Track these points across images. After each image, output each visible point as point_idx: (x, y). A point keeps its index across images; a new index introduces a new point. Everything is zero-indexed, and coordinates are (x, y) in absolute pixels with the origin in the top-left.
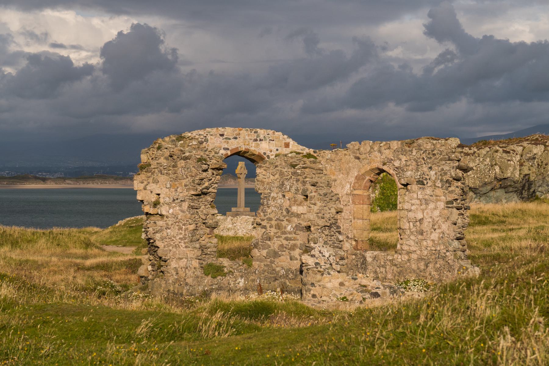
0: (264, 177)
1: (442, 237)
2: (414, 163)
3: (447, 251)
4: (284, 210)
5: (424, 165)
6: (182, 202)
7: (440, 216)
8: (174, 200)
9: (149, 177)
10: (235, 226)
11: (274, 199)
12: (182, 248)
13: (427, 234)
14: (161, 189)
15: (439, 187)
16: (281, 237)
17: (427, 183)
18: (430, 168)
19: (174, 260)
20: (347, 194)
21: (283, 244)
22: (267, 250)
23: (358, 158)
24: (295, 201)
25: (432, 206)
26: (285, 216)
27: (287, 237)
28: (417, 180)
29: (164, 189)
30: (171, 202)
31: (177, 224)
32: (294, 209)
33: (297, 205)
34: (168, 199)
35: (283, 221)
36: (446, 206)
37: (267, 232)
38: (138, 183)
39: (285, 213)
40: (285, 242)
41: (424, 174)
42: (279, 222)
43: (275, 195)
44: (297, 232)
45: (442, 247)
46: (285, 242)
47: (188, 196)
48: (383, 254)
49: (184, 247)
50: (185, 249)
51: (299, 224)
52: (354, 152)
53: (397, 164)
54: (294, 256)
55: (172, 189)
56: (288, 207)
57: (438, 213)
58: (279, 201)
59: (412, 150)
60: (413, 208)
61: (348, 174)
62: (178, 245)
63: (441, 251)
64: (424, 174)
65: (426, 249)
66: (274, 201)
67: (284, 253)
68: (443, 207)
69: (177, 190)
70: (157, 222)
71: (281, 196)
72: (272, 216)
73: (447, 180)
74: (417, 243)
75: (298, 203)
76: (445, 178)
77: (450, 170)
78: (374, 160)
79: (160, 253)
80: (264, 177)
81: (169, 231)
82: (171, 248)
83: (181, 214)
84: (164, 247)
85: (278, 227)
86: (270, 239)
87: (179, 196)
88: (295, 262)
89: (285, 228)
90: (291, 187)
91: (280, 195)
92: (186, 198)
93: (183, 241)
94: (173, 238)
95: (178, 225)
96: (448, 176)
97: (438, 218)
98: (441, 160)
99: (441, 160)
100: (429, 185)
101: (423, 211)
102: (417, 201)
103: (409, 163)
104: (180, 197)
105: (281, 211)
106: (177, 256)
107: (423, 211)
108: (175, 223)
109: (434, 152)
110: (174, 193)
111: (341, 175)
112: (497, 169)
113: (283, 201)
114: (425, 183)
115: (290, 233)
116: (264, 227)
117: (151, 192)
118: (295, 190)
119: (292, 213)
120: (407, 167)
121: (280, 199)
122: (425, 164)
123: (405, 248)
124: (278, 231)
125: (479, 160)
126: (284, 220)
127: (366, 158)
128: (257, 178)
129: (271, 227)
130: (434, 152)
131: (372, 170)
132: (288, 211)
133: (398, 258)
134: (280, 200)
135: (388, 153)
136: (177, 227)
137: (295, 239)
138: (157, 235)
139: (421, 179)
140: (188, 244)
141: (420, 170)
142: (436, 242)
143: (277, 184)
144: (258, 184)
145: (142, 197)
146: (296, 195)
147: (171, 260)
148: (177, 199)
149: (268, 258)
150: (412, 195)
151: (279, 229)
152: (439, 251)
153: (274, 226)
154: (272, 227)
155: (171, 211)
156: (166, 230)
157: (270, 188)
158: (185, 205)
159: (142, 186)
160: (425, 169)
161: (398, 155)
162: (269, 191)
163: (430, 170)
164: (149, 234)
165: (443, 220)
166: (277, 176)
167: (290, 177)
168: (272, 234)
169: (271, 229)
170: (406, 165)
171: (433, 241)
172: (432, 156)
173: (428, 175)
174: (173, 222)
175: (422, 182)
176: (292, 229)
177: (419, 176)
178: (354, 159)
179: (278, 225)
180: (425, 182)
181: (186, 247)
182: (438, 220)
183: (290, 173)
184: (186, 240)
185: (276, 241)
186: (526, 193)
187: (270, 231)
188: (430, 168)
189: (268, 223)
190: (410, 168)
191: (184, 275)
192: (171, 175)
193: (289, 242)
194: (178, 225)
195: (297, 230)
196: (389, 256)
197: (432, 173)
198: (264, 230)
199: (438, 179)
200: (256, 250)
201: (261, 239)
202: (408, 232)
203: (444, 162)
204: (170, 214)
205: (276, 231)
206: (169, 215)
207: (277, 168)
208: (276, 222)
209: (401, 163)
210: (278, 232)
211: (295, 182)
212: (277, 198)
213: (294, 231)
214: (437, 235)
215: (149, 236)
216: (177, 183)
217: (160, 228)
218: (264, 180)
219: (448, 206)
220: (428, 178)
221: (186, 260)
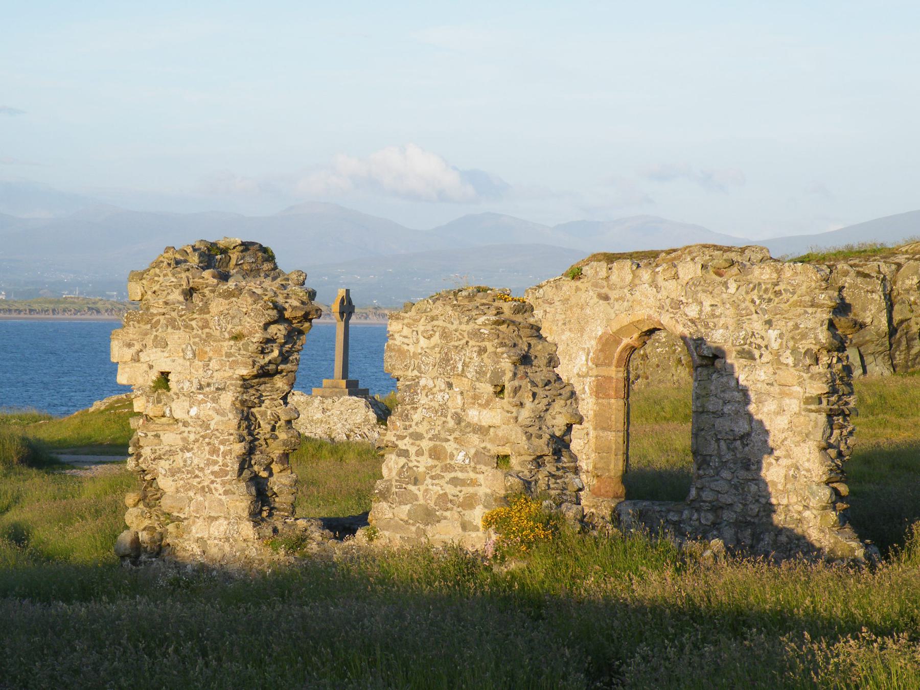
0: (406, 341)
1: (795, 477)
2: (731, 311)
3: (806, 507)
4: (449, 417)
5: (755, 316)
6: (220, 392)
7: (790, 429)
8: (201, 387)
9: (146, 334)
10: (329, 416)
11: (429, 392)
12: (217, 495)
14: (174, 361)
15: (787, 365)
16: (443, 477)
17: (761, 356)
18: (769, 323)
19: (200, 522)
21: (445, 494)
22: (408, 507)
23: (606, 298)
24: (476, 397)
26: (451, 431)
28: (739, 348)
29: (181, 361)
30: (193, 390)
31: (207, 440)
32: (473, 415)
33: (480, 405)
34: (187, 384)
36: (803, 406)
37: (411, 465)
38: (120, 347)
39: (451, 423)
40: (451, 490)
41: (753, 334)
42: (438, 443)
43: (430, 384)
44: (478, 467)
45: (794, 499)
46: (451, 490)
47: (233, 379)
48: (658, 508)
49: (221, 491)
50: (223, 498)
51: (484, 448)
52: (596, 285)
53: (692, 311)
54: (471, 523)
55: (196, 362)
56: (459, 411)
57: (786, 422)
58: (439, 397)
61: (582, 330)
62: (208, 486)
63: (791, 508)
64: (753, 334)
65: (757, 501)
66: (427, 396)
67: (448, 514)
68: (797, 410)
69: (208, 365)
70: (161, 433)
71: (443, 386)
72: (421, 429)
73: (808, 350)
74: (736, 488)
75: (483, 401)
76: (803, 346)
77: (815, 329)
78: (640, 303)
79: (166, 503)
80: (406, 341)
81: (188, 455)
82: (191, 494)
83: (217, 418)
84: (177, 491)
87: (211, 377)
88: (474, 534)
89: (452, 456)
90: (465, 365)
92: (228, 383)
93: (219, 480)
94: (197, 472)
95: (209, 444)
96: (809, 341)
97: (786, 434)
98: (795, 304)
99: (795, 304)
100: (764, 359)
104: (214, 380)
105: (444, 419)
106: (205, 513)
108: (204, 437)
109: (777, 288)
110: (201, 371)
111: (568, 334)
113: (447, 396)
114: (757, 356)
115: (463, 469)
116: (405, 453)
117: (151, 367)
118: (477, 372)
119: (469, 425)
120: (716, 320)
121: (441, 391)
122: (756, 312)
123: (707, 495)
124: (436, 462)
126: (449, 440)
127: (621, 299)
128: (390, 342)
129: (419, 453)
130: (777, 288)
131: (635, 324)
132: (459, 419)
133: (691, 519)
134: (442, 394)
135: (672, 289)
136: (207, 448)
137: (474, 483)
138: (162, 463)
139: (746, 347)
140: (231, 487)
141: (745, 326)
143: (436, 356)
144: (390, 357)
145: (130, 378)
146: (478, 385)
147: (191, 521)
149: (413, 525)
150: (725, 380)
151: (438, 459)
152: (787, 506)
153: (426, 454)
154: (422, 455)
155: (194, 411)
156: (180, 453)
157: (419, 367)
159: (128, 353)
160: (757, 325)
161: (696, 292)
162: (416, 373)
163: (767, 326)
164: (144, 462)
165: (798, 438)
166: (436, 339)
167: (464, 341)
168: (422, 469)
169: (419, 459)
170: (713, 316)
172: (772, 297)
173: (762, 338)
174: (197, 437)
176: (467, 461)
177: (744, 339)
178: (596, 299)
179: (435, 451)
180: (757, 354)
181: (226, 493)
182: (786, 439)
183: (465, 334)
184: (229, 477)
185: (430, 487)
186: (902, 357)
187: (416, 464)
188: (769, 323)
189: (412, 444)
190: (722, 321)
192: (195, 331)
193: (459, 488)
194: (209, 444)
195: (478, 463)
196: (672, 514)
197: (773, 334)
198: (403, 460)
199: (787, 347)
200: (384, 505)
201: (396, 481)
202: (715, 462)
203: (800, 310)
204: (191, 417)
205: (431, 462)
206: (189, 420)
207: (435, 323)
209: (701, 311)
210: (436, 466)
211: (475, 355)
212: (435, 390)
213: (472, 464)
214: (782, 472)
215: (144, 466)
216: (208, 349)
217: (167, 448)
218: (406, 347)
219: (809, 407)
220: (763, 344)
221: (226, 522)
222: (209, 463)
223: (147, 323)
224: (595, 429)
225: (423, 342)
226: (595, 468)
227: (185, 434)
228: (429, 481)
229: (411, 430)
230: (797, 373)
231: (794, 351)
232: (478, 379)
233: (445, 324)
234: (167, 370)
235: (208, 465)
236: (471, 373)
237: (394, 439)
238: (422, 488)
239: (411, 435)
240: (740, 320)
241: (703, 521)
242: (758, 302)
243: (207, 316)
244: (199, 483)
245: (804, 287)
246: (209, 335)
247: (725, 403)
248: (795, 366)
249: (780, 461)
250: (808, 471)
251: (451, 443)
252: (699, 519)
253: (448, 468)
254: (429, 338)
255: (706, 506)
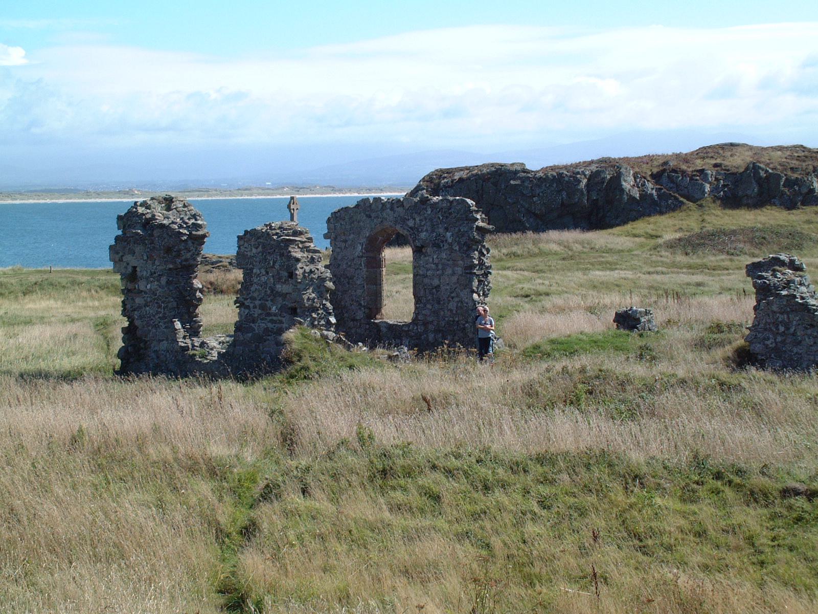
3: (467, 322)
8: (152, 274)
13: (444, 303)
17: (443, 245)
20: (358, 257)
23: (370, 217)
25: (449, 271)
27: (272, 320)
32: (279, 287)
33: (282, 282)
35: (267, 301)
40: (270, 325)
46: (270, 325)
53: (411, 223)
59: (426, 208)
60: (429, 273)
67: (269, 338)
71: (264, 273)
72: (255, 295)
81: (147, 308)
82: (150, 328)
83: (160, 290)
84: (143, 327)
85: (263, 307)
86: (254, 322)
87: (156, 269)
89: (270, 309)
90: (274, 262)
91: (263, 271)
100: (445, 248)
101: (439, 277)
102: (432, 265)
103: (423, 223)
107: (439, 277)
108: (154, 299)
109: (450, 211)
112: (564, 194)
115: (275, 315)
117: (128, 264)
125: (546, 185)
129: (255, 307)
130: (450, 211)
132: (272, 290)
138: (136, 312)
142: (454, 312)
146: (281, 272)
148: (155, 273)
150: (427, 258)
153: (258, 307)
156: (144, 308)
158: (164, 280)
160: (441, 231)
166: (260, 249)
168: (256, 315)
171: (451, 311)
175: (438, 244)
181: (166, 327)
189: (251, 303)
191: (165, 359)
194: (157, 303)
197: (449, 234)
198: (247, 311)
203: (461, 222)
205: (260, 312)
207: (259, 240)
208: (260, 302)
211: (278, 257)
222: (158, 313)
223: (125, 242)
224: (367, 284)
225: (254, 250)
226: (368, 304)
227: (145, 298)
228: (259, 321)
229: (250, 296)
230: (460, 255)
231: (459, 243)
232: (280, 270)
233: (264, 241)
234: (136, 265)
235: (156, 314)
236: (277, 266)
237: (243, 300)
238: (257, 325)
239: (250, 298)
240: (433, 228)
241: (419, 330)
242: (441, 218)
243: (153, 238)
244: (153, 323)
245: (462, 211)
246: (154, 248)
247: (427, 270)
248: (459, 251)
249: (454, 299)
250: (467, 303)
251: (269, 302)
252: (417, 329)
253: (269, 314)
254: (257, 248)
255: (421, 323)
